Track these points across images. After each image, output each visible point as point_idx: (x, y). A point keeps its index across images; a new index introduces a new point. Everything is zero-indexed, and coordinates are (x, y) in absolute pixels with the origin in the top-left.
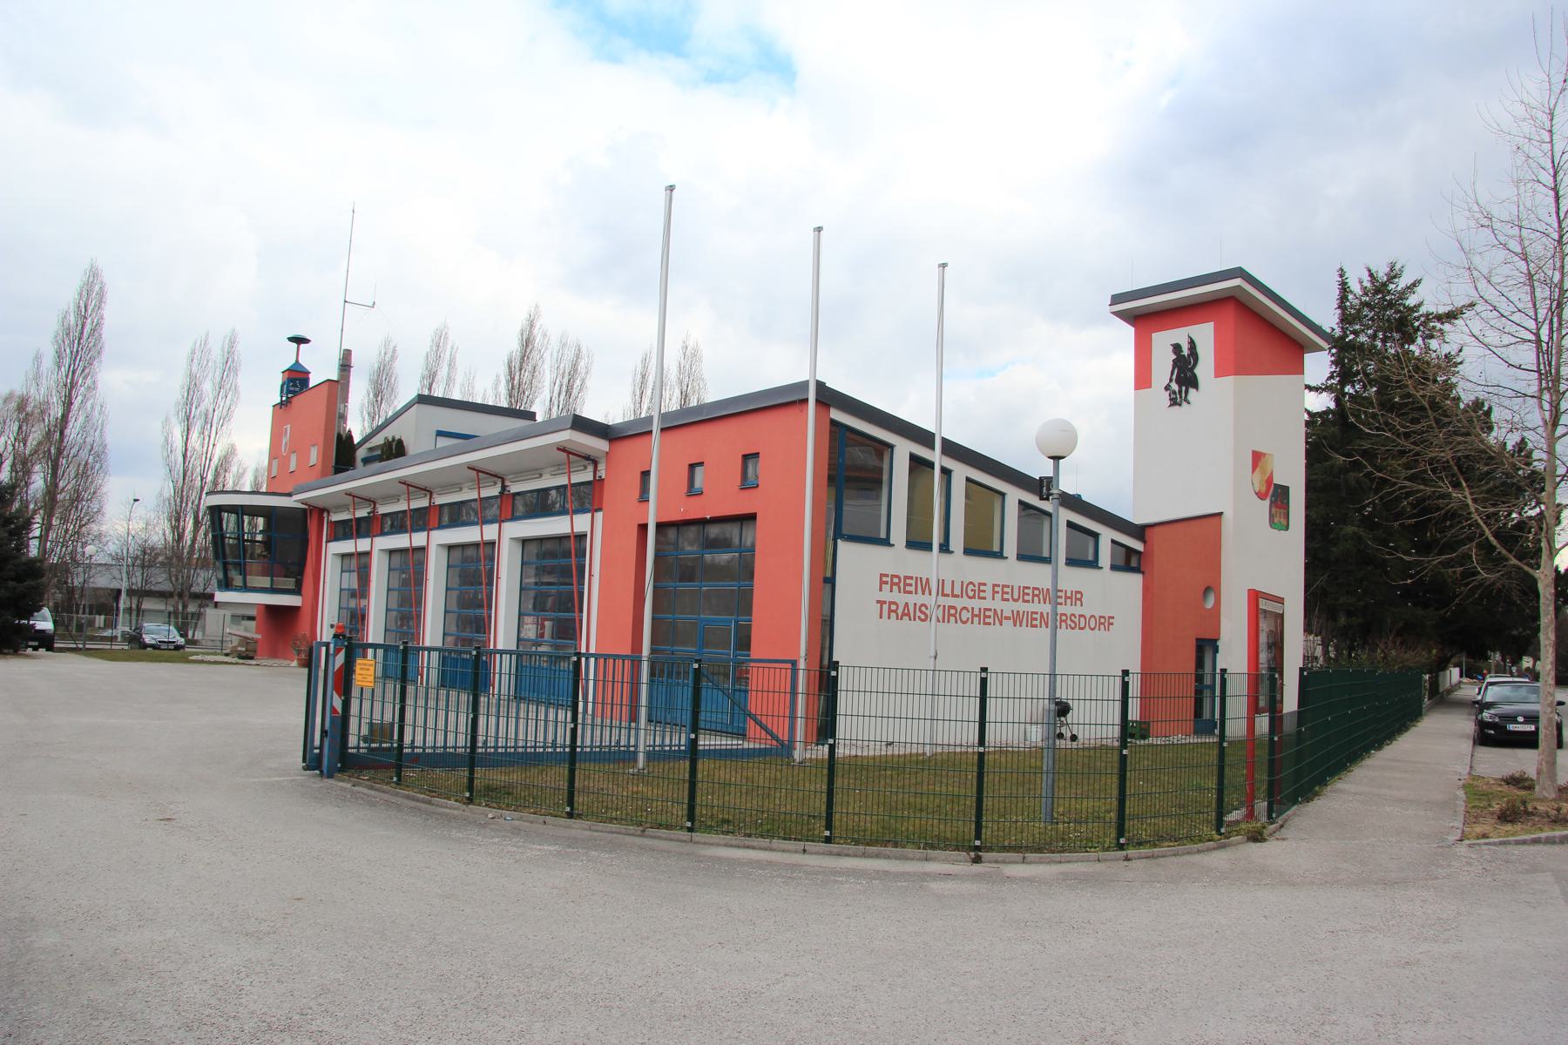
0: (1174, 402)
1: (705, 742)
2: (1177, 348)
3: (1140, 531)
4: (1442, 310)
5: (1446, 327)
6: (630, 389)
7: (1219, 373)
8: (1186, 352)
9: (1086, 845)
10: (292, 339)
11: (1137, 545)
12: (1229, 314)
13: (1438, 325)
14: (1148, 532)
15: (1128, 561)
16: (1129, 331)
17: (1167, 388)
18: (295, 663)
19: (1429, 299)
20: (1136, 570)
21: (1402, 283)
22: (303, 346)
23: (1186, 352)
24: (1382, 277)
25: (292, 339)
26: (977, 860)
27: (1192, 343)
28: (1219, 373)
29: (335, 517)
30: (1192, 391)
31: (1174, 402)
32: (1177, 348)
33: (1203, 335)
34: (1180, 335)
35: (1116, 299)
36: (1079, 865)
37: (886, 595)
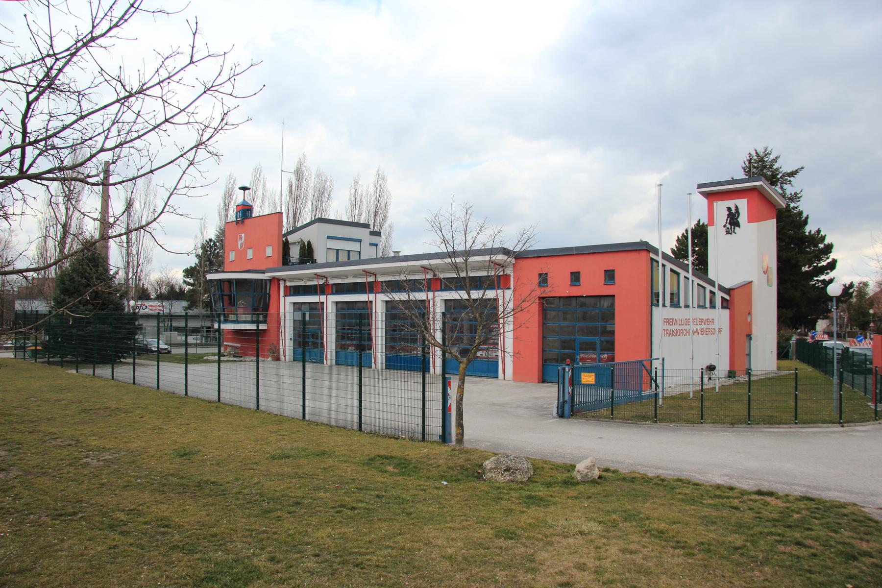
0: (728, 233)
1: (618, 393)
2: (729, 209)
3: (728, 291)
4: (789, 171)
5: (792, 179)
6: (348, 197)
7: (750, 221)
8: (733, 211)
9: (779, 423)
10: (240, 188)
11: (727, 297)
12: (755, 196)
13: (789, 179)
14: (731, 292)
15: (725, 304)
16: (705, 201)
17: (725, 226)
18: (270, 359)
19: (785, 166)
20: (726, 308)
21: (772, 157)
22: (247, 191)
23: (733, 211)
24: (762, 154)
25: (240, 188)
26: (843, 426)
27: (737, 208)
28: (750, 221)
29: (289, 284)
30: (737, 228)
31: (728, 233)
32: (729, 209)
33: (742, 204)
34: (731, 203)
35: (700, 186)
36: (783, 429)
37: (666, 327)
